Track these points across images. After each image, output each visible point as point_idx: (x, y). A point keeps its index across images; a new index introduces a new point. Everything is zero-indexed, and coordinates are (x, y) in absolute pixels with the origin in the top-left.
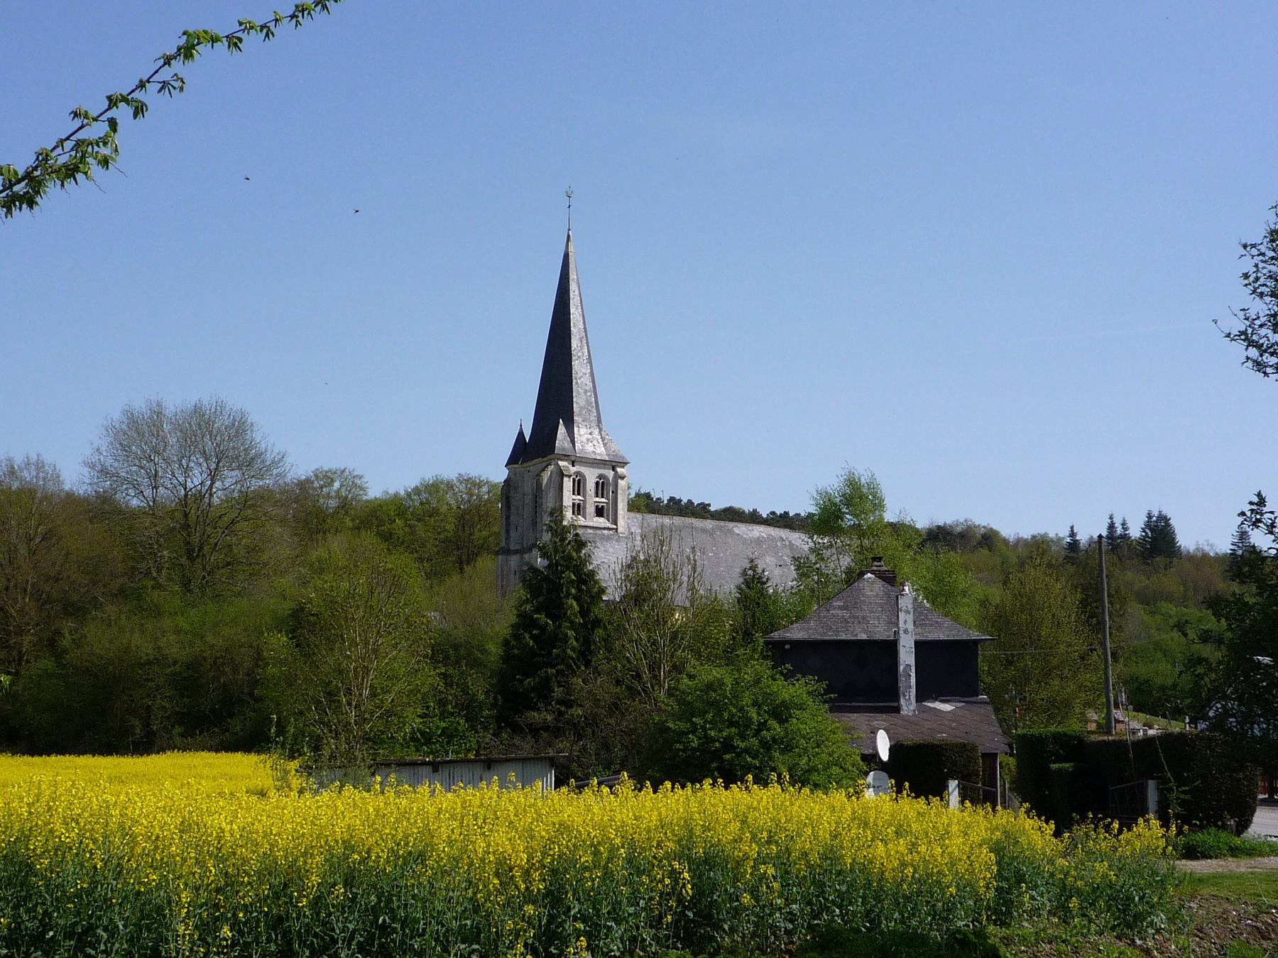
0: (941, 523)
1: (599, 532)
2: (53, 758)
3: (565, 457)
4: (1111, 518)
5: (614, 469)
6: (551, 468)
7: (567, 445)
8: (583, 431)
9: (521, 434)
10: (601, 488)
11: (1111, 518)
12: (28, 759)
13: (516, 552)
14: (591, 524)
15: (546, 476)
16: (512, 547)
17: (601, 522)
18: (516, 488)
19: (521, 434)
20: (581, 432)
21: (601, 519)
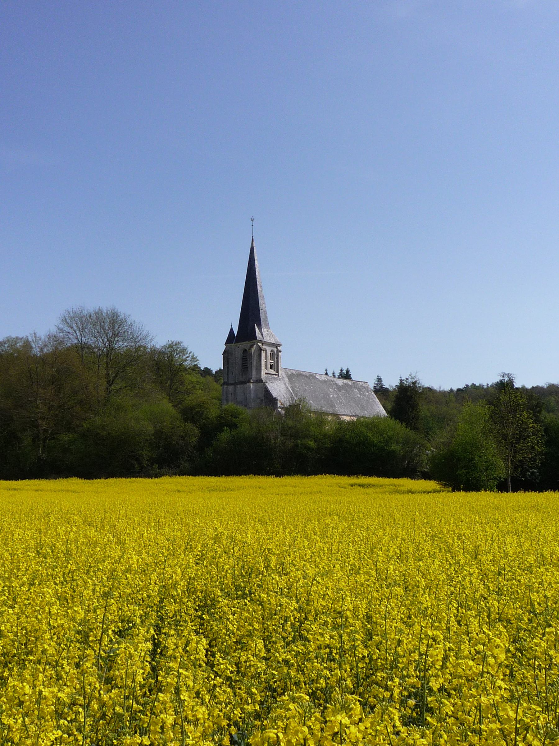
0: (552, 383)
1: (273, 376)
2: (138, 479)
3: (261, 341)
4: (326, 371)
5: (277, 348)
6: (255, 346)
7: (261, 336)
8: (265, 330)
9: (232, 330)
10: (272, 355)
11: (326, 371)
12: (123, 480)
13: (232, 384)
14: (269, 372)
15: (253, 349)
16: (230, 382)
17: (272, 371)
18: (231, 355)
19: (232, 330)
20: (264, 330)
21: (272, 370)
